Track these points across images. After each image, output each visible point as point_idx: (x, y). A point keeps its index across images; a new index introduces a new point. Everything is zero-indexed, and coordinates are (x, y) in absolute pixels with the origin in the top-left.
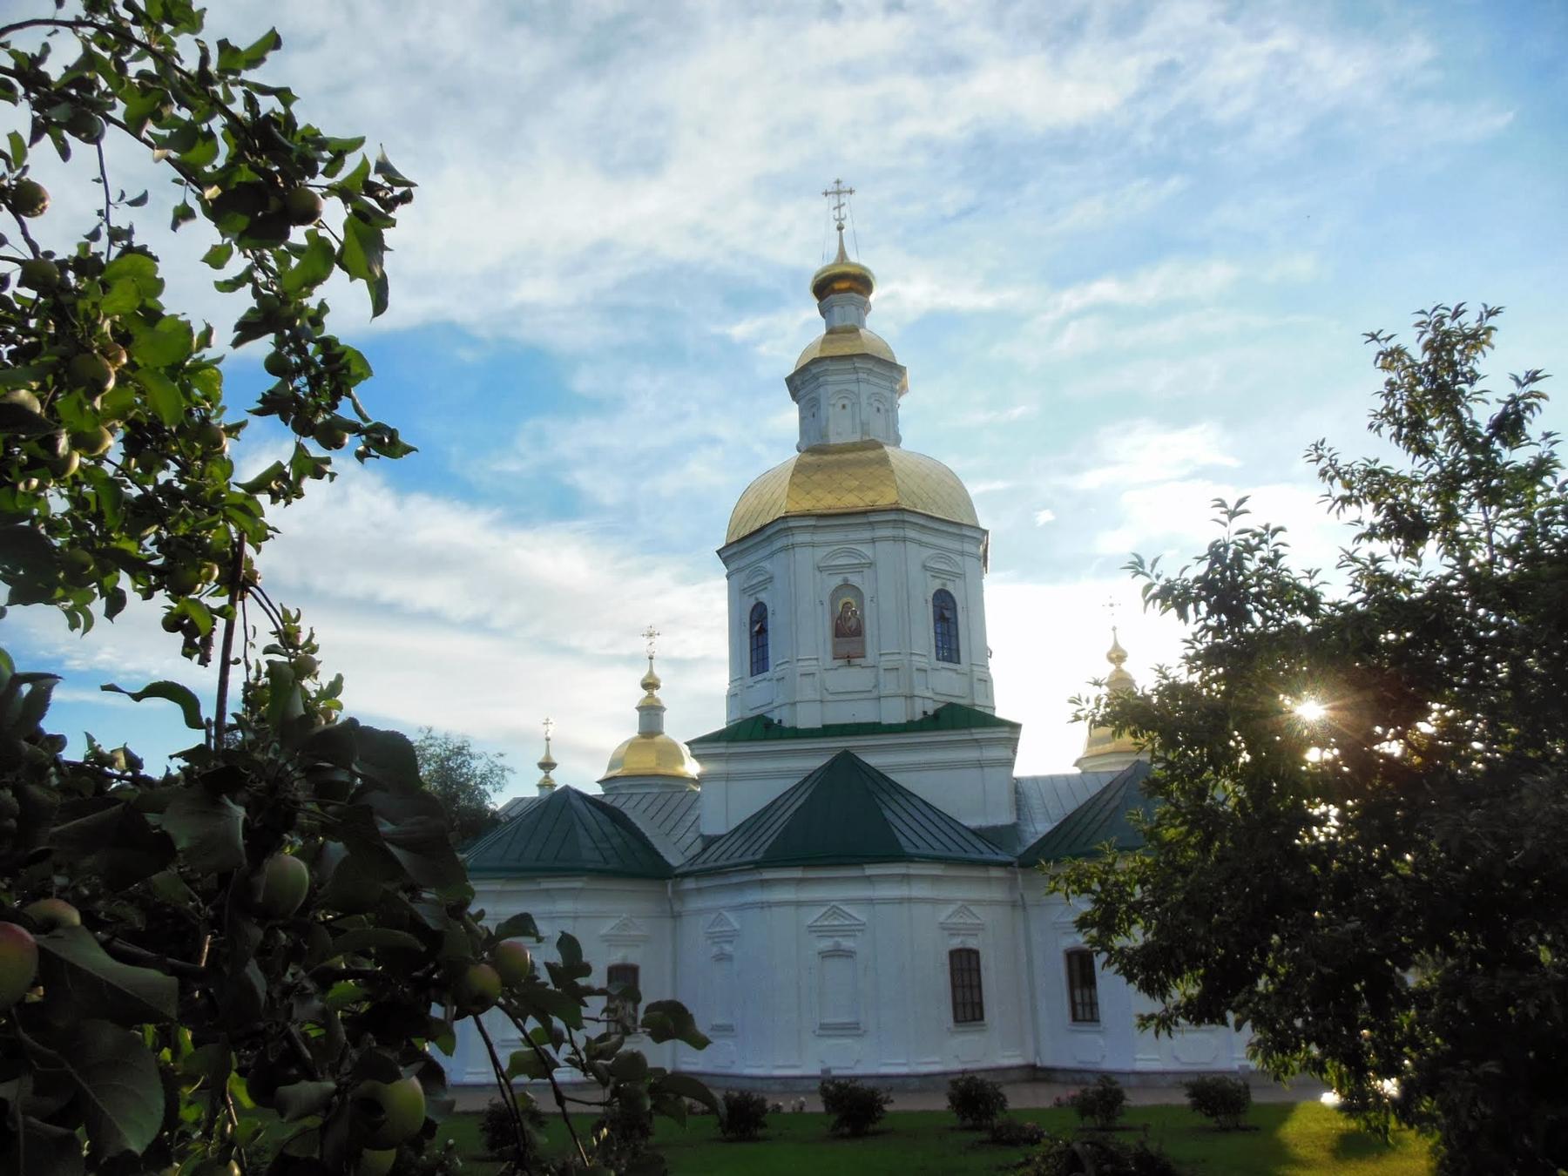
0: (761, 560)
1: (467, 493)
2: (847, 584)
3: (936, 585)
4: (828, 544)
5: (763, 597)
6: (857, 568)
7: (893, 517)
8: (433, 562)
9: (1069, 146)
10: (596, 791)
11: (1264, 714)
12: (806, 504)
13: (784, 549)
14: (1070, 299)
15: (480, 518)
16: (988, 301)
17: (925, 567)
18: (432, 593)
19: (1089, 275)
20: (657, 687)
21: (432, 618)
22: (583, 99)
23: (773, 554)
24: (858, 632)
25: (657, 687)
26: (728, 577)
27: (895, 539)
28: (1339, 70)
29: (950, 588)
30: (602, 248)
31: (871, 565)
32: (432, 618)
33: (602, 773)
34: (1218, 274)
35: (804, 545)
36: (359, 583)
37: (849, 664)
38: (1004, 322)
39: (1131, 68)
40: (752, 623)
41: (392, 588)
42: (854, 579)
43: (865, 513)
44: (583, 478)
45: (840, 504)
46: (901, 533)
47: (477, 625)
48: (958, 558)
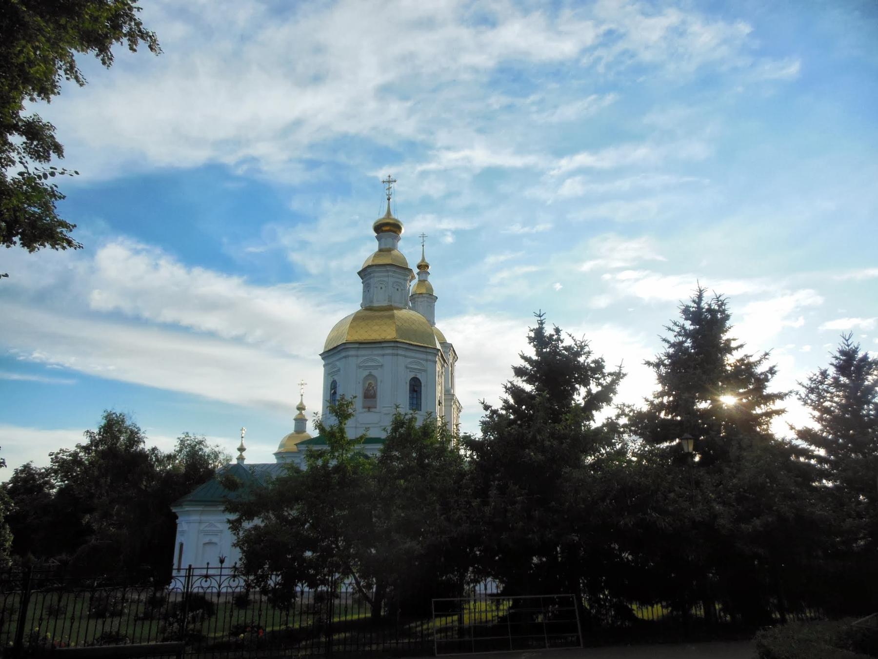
0: (378, 355)
1: (225, 265)
2: (370, 375)
3: (412, 375)
4: (363, 356)
5: (336, 378)
6: (375, 368)
7: (392, 345)
8: (211, 305)
9: (557, 72)
10: (274, 461)
11: (715, 384)
12: (357, 337)
13: (345, 357)
14: (566, 164)
15: (235, 281)
16: (517, 162)
17: (407, 368)
18: (210, 322)
19: (573, 151)
20: (304, 409)
21: (211, 336)
22: (278, 35)
23: (383, 355)
24: (374, 396)
25: (304, 409)
26: (324, 366)
27: (393, 355)
28: (706, 37)
29: (419, 376)
30: (298, 123)
31: (382, 366)
32: (211, 336)
33: (276, 449)
34: (641, 153)
35: (352, 356)
36: (169, 315)
37: (369, 411)
38: (530, 175)
39: (588, 33)
40: (331, 389)
41: (188, 318)
42: (374, 372)
43: (380, 342)
44: (295, 257)
45: (369, 338)
46: (395, 352)
47: (238, 341)
48: (424, 362)
